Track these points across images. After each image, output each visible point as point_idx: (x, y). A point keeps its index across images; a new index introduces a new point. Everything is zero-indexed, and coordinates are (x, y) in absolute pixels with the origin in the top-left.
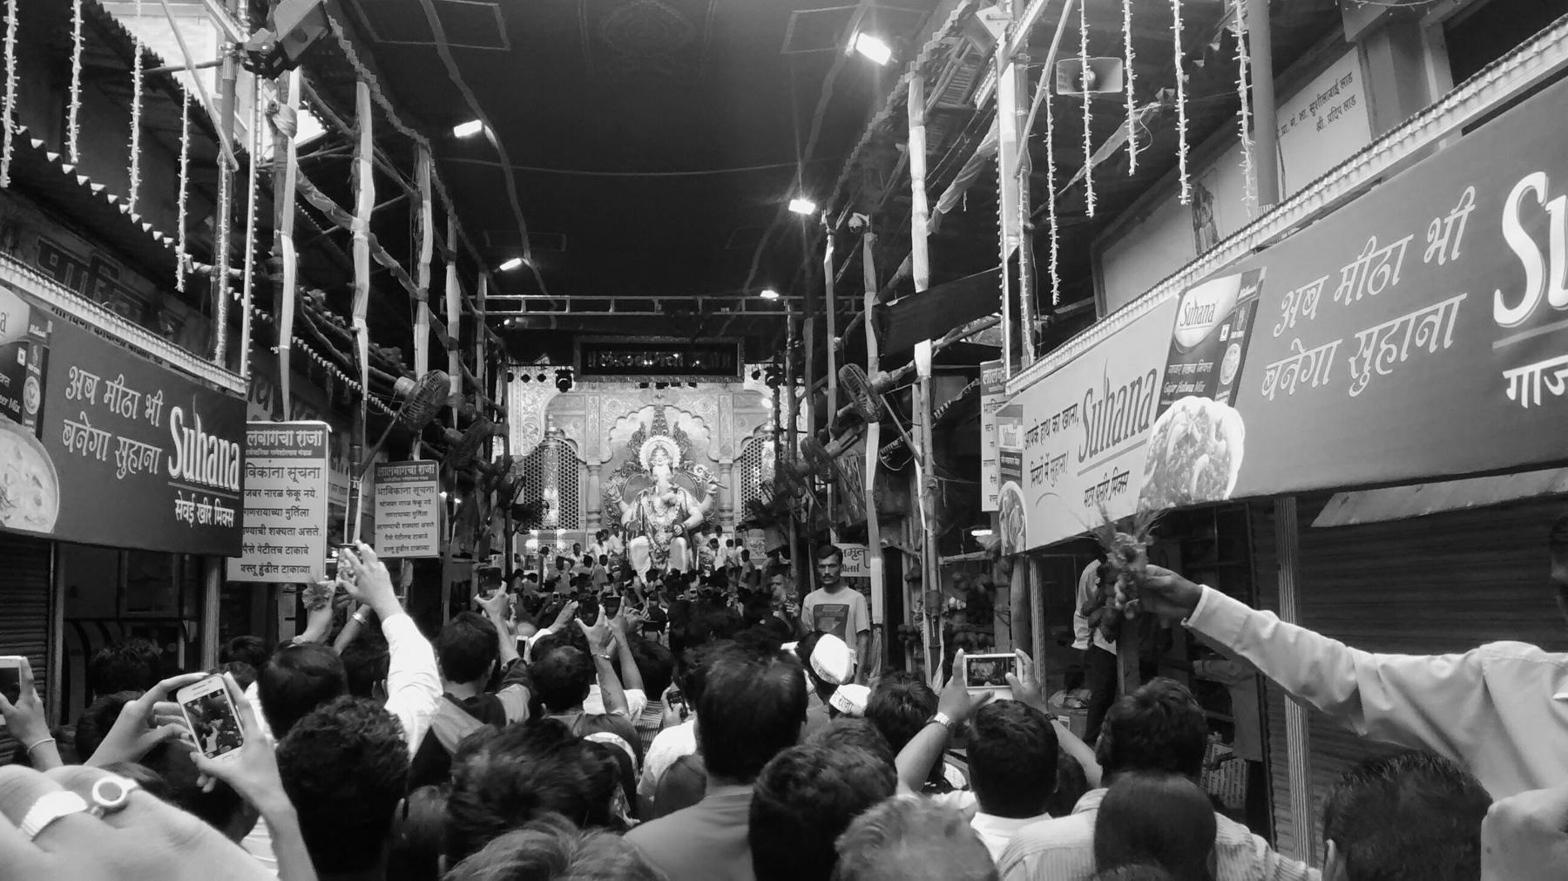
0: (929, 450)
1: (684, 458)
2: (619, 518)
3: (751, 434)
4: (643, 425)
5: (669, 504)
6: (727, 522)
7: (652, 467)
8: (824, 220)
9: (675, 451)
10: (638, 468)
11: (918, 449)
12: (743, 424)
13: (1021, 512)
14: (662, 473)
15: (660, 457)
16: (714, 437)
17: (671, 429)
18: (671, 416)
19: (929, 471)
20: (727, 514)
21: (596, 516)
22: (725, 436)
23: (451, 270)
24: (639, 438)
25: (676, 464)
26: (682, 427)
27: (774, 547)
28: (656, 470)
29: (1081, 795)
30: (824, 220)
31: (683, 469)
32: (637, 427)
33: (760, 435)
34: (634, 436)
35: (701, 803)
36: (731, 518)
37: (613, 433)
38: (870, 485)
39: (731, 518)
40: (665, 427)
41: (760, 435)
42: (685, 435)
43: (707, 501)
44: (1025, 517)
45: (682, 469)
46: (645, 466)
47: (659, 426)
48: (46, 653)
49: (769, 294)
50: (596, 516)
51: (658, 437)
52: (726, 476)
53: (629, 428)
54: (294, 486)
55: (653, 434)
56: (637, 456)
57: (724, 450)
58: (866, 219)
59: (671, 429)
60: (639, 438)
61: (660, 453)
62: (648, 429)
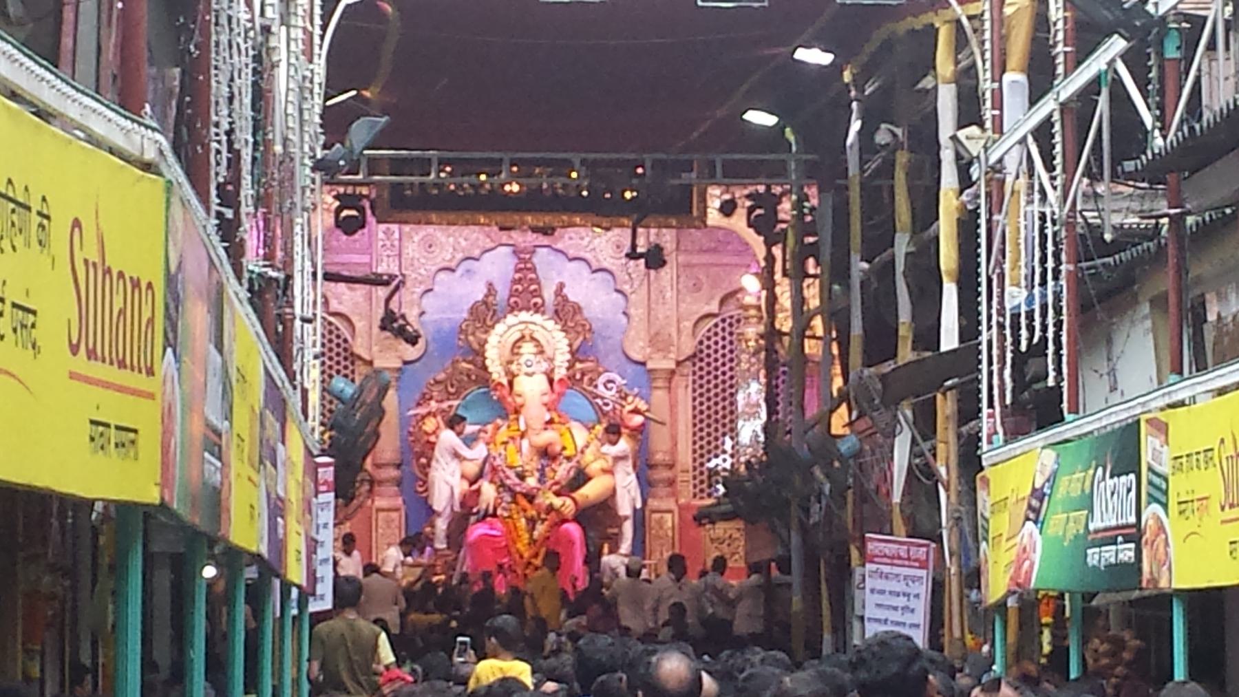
0: (954, 474)
1: (576, 355)
3: (714, 307)
4: (490, 286)
5: (546, 454)
6: (662, 490)
7: (512, 377)
8: (847, 76)
9: (559, 343)
10: (482, 377)
11: (943, 471)
12: (697, 287)
13: (1167, 544)
14: (531, 388)
15: (526, 355)
16: (637, 312)
17: (549, 294)
18: (553, 271)
19: (953, 498)
20: (665, 474)
21: (393, 473)
22: (661, 312)
24: (485, 314)
25: (560, 373)
26: (572, 294)
27: (766, 555)
28: (522, 384)
30: (847, 76)
31: (574, 380)
33: (731, 310)
34: (473, 310)
36: (671, 483)
37: (428, 301)
38: (897, 498)
40: (537, 293)
41: (731, 310)
42: (577, 309)
44: (1171, 550)
45: (572, 380)
47: (525, 292)
48: (909, 559)
49: (760, 118)
50: (393, 473)
52: (660, 396)
54: (908, 590)
55: (513, 308)
56: (478, 354)
57: (657, 341)
58: (899, 131)
59: (549, 294)
61: (528, 348)
62: (502, 292)
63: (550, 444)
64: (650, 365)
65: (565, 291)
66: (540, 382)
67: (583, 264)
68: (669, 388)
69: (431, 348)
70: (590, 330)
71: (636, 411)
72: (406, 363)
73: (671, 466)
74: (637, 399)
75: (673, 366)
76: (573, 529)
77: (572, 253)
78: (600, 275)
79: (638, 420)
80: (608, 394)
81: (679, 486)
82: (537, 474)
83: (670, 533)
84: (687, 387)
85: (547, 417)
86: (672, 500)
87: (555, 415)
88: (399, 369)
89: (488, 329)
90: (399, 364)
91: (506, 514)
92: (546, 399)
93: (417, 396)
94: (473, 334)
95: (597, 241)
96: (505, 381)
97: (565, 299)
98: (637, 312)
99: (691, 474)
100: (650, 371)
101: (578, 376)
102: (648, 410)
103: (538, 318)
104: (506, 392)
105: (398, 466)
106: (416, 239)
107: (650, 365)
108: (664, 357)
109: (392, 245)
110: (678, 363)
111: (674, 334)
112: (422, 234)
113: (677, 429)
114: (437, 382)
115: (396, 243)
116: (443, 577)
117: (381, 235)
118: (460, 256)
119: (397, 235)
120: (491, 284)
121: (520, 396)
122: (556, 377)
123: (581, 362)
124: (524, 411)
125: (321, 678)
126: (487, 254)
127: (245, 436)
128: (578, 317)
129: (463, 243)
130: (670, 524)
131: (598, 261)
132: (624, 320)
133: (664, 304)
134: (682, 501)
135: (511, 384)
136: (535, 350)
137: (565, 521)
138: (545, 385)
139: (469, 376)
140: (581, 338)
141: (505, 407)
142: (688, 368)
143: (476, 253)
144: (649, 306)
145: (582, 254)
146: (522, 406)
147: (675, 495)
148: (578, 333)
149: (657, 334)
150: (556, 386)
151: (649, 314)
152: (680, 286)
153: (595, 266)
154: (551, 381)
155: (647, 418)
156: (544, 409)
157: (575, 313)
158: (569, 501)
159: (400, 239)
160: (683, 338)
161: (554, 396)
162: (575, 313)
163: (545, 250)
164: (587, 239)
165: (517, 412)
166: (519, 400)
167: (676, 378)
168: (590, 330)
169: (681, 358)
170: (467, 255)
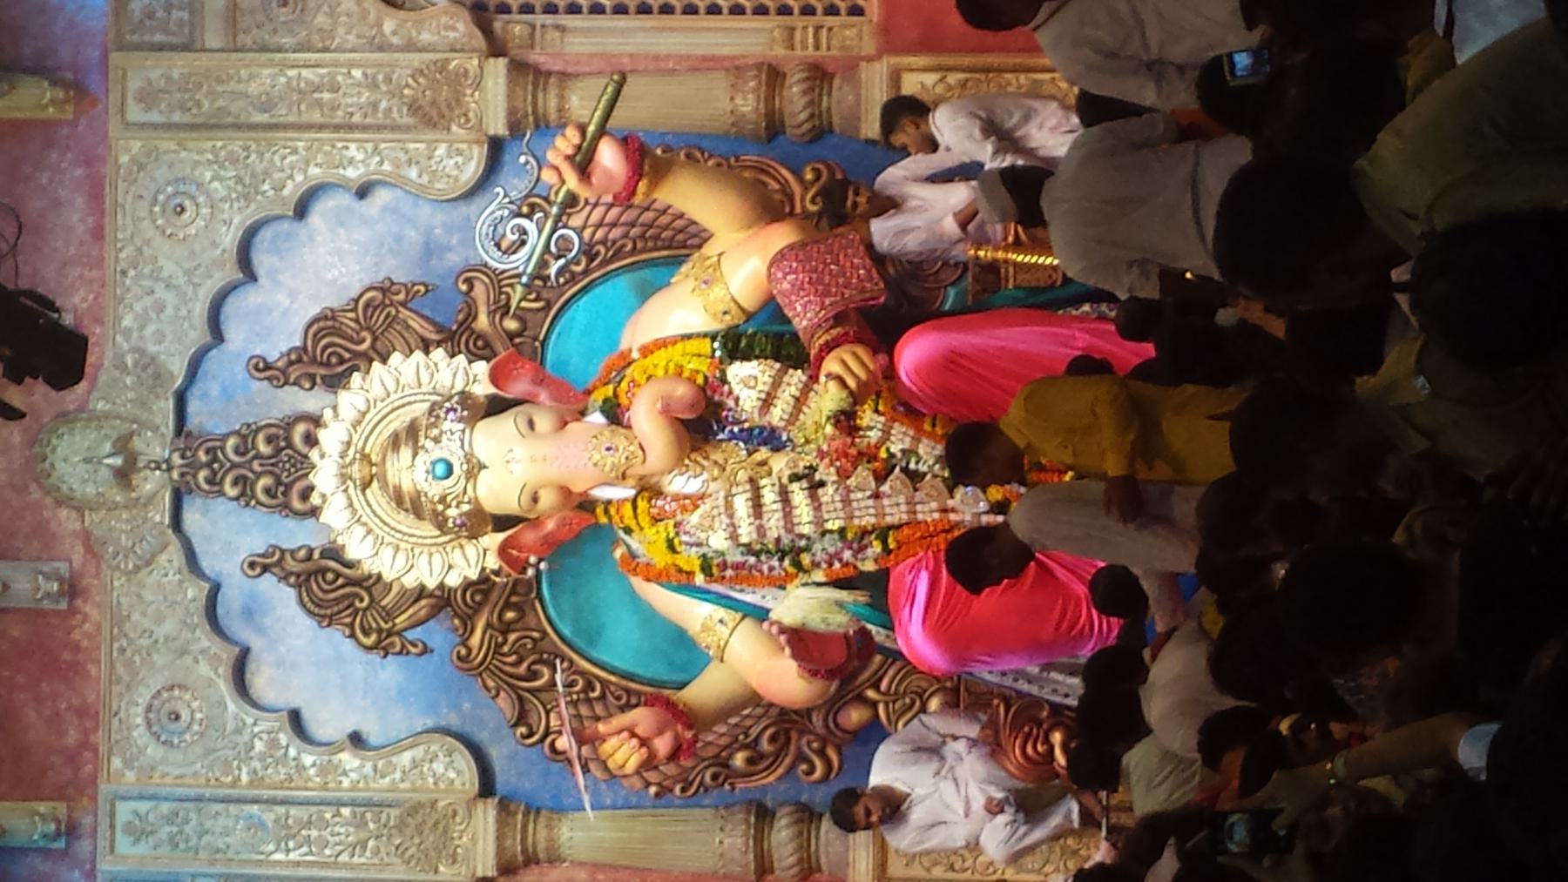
1: (458, 337)
2: (788, 721)
5: (701, 423)
6: (839, 98)
7: (479, 521)
14: (515, 463)
16: (358, 161)
21: (782, 834)
23: (1440, 32)
25: (478, 378)
26: (283, 340)
28: (499, 490)
29: (1140, 711)
31: (512, 344)
32: (281, 597)
35: (969, 29)
36: (819, 75)
37: (328, 723)
39: (819, 75)
40: (280, 434)
42: (325, 324)
43: (692, 197)
46: (472, 559)
47: (274, 468)
50: (782, 834)
51: (324, 477)
53: (306, 660)
56: (442, 600)
57: (433, 112)
60: (333, 589)
63: (666, 411)
64: (498, 127)
65: (272, 356)
66: (496, 440)
67: (230, 307)
68: (564, 76)
69: (453, 720)
70: (383, 290)
71: (583, 163)
72: (487, 787)
73: (774, 75)
74: (551, 156)
75: (501, 63)
76: (915, 352)
77: (197, 334)
78: (262, 260)
79: (609, 156)
80: (536, 241)
81: (830, 52)
82: (763, 453)
83: (953, 78)
84: (562, 29)
85: (597, 418)
86: (864, 69)
87: (598, 397)
88: (504, 807)
89: (371, 583)
90: (487, 814)
91: (877, 547)
92: (544, 422)
93: (556, 767)
94: (389, 615)
95: (169, 268)
96: (493, 540)
97: (298, 357)
98: (358, 161)
99: (797, 21)
100: (516, 128)
101: (511, 325)
102: (582, 129)
103: (331, 437)
104: (529, 537)
105: (763, 815)
106: (153, 751)
107: (498, 127)
108: (478, 86)
109: (171, 818)
110: (496, 48)
111: (417, 59)
112: (140, 735)
113: (681, 58)
114: (521, 719)
115: (165, 807)
116: (1057, 737)
117: (143, 849)
118: (204, 639)
119: (143, 807)
120: (252, 565)
121: (535, 500)
122: (483, 390)
123: (472, 315)
124: (578, 488)
125: (1282, 833)
126: (205, 564)
127: (895, 775)
128: (347, 320)
129: (169, 627)
130: (930, 79)
131: (219, 263)
132: (382, 196)
133: (335, 89)
134: (869, 46)
135: (502, 522)
136: (406, 452)
137: (890, 372)
138: (505, 426)
139: (506, 629)
140: (404, 313)
141: (576, 532)
142: (514, 28)
143: (195, 592)
144: (337, 128)
145: (200, 309)
146: (565, 492)
147: (851, 66)
148: (391, 321)
149: (414, 108)
150: (517, 389)
151: (365, 128)
152: (287, 41)
153: (232, 273)
154: (496, 406)
155: (602, 132)
156: (573, 427)
157: (336, 331)
158: (831, 365)
159: (153, 797)
160: (426, 37)
161: (543, 396)
162: (336, 331)
163: (194, 406)
164: (161, 292)
165: (586, 505)
166: (547, 499)
167: (536, 57)
168: (383, 290)
169: (479, 41)
170: (198, 618)
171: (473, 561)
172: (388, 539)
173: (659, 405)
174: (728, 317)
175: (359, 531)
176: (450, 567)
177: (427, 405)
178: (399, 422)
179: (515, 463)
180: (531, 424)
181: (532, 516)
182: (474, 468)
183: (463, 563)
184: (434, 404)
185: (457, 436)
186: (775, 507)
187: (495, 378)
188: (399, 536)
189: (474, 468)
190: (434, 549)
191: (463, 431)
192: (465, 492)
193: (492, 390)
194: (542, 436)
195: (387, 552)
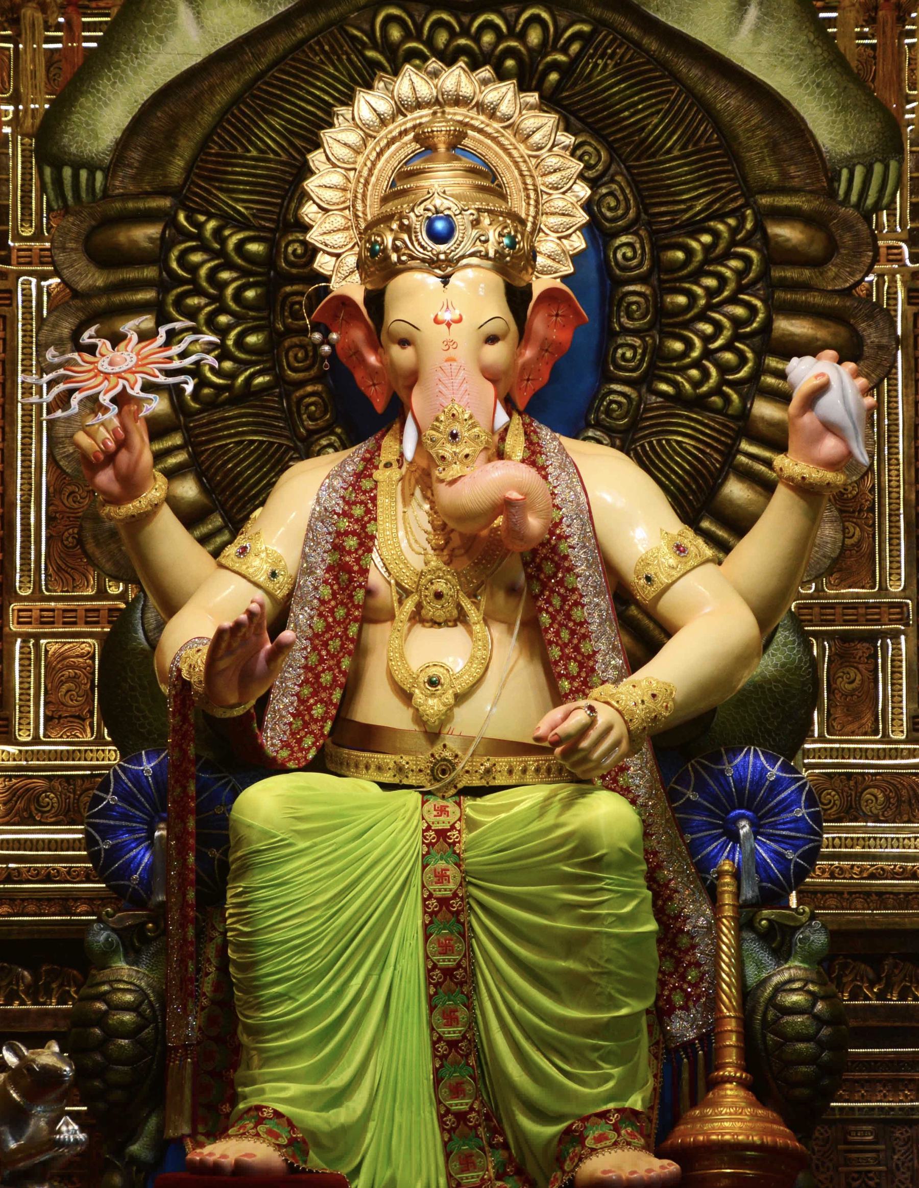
14: (450, 315)
28: (417, 298)
63: (506, 506)
66: (474, 296)
92: (496, 354)
121: (404, 342)
135: (376, 301)
146: (413, 377)
150: (539, 324)
154: (517, 298)
166: (402, 356)
171: (329, 239)
172: (361, 159)
173: (515, 495)
174: (643, 581)
175: (385, 107)
176: (326, 211)
177: (523, 216)
178: (509, 177)
179: (450, 315)
180: (492, 339)
181: (384, 337)
182: (444, 267)
183: (327, 226)
184: (523, 222)
185: (479, 247)
186: (103, 433)
187: (550, 295)
188: (365, 173)
189: (444, 267)
190: (349, 195)
191: (486, 257)
192: (412, 258)
193: (537, 291)
194: (478, 349)
195: (336, 178)
